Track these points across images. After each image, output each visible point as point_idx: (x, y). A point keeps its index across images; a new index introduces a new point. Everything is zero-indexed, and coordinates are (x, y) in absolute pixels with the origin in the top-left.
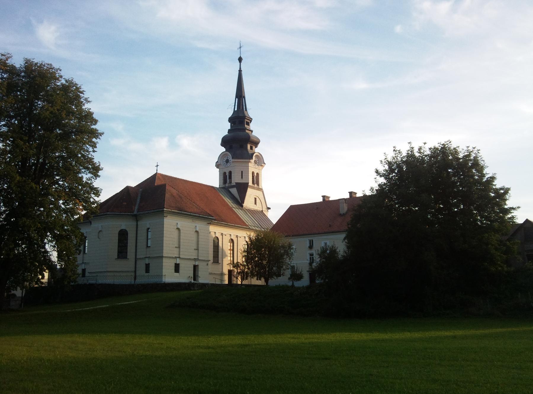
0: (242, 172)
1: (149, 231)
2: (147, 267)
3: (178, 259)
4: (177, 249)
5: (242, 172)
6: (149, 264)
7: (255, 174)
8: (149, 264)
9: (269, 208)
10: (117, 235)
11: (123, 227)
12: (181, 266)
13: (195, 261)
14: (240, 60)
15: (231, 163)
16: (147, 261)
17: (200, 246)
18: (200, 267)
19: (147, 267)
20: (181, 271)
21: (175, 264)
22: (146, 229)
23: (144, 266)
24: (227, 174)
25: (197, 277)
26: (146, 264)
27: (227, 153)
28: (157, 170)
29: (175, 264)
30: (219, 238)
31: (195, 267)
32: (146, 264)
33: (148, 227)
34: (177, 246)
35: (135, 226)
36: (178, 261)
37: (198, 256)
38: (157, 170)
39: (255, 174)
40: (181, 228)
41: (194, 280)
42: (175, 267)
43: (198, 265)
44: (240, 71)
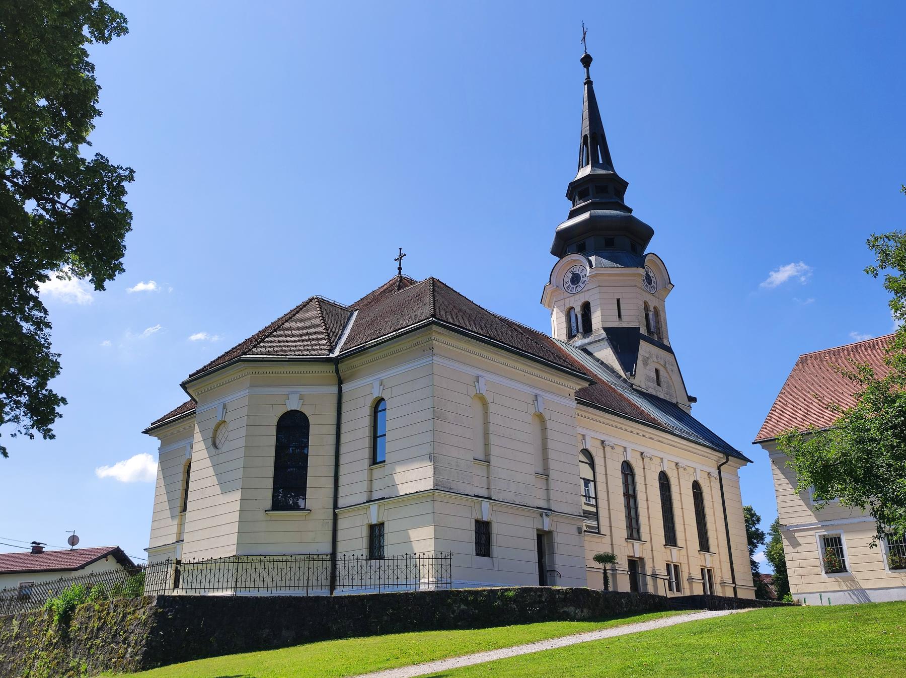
0: (618, 301)
1: (379, 409)
2: (376, 533)
3: (486, 504)
4: (480, 470)
5: (618, 301)
6: (382, 525)
7: (652, 309)
8: (382, 525)
9: (693, 400)
10: (273, 431)
11: (293, 405)
12: (495, 529)
13: (541, 515)
14: (587, 61)
15: (586, 282)
16: (374, 515)
17: (552, 465)
18: (558, 538)
19: (376, 533)
20: (495, 550)
21: (477, 522)
22: (369, 401)
23: (365, 532)
24: (578, 309)
25: (548, 574)
26: (372, 527)
27: (577, 258)
28: (400, 269)
29: (477, 522)
30: (594, 454)
31: (544, 539)
32: (372, 527)
33: (376, 394)
34: (482, 457)
35: (334, 400)
36: (486, 512)
37: (548, 500)
38: (400, 269)
39: (652, 309)
40: (489, 398)
41: (542, 581)
42: (478, 532)
43: (550, 533)
44: (589, 83)
